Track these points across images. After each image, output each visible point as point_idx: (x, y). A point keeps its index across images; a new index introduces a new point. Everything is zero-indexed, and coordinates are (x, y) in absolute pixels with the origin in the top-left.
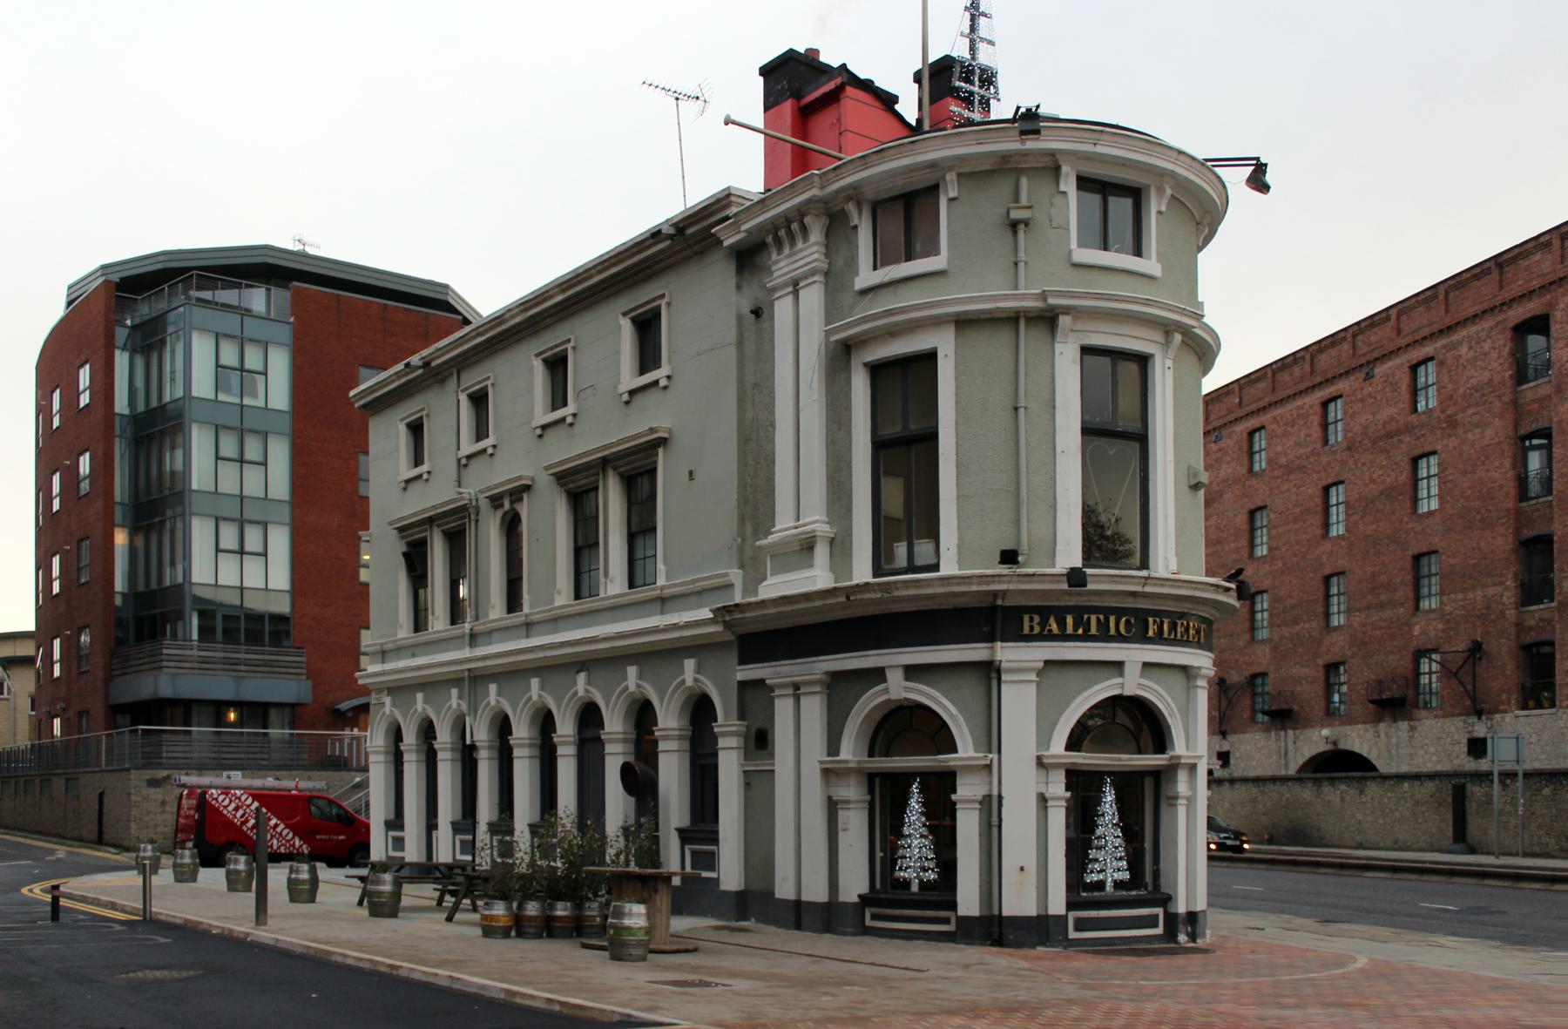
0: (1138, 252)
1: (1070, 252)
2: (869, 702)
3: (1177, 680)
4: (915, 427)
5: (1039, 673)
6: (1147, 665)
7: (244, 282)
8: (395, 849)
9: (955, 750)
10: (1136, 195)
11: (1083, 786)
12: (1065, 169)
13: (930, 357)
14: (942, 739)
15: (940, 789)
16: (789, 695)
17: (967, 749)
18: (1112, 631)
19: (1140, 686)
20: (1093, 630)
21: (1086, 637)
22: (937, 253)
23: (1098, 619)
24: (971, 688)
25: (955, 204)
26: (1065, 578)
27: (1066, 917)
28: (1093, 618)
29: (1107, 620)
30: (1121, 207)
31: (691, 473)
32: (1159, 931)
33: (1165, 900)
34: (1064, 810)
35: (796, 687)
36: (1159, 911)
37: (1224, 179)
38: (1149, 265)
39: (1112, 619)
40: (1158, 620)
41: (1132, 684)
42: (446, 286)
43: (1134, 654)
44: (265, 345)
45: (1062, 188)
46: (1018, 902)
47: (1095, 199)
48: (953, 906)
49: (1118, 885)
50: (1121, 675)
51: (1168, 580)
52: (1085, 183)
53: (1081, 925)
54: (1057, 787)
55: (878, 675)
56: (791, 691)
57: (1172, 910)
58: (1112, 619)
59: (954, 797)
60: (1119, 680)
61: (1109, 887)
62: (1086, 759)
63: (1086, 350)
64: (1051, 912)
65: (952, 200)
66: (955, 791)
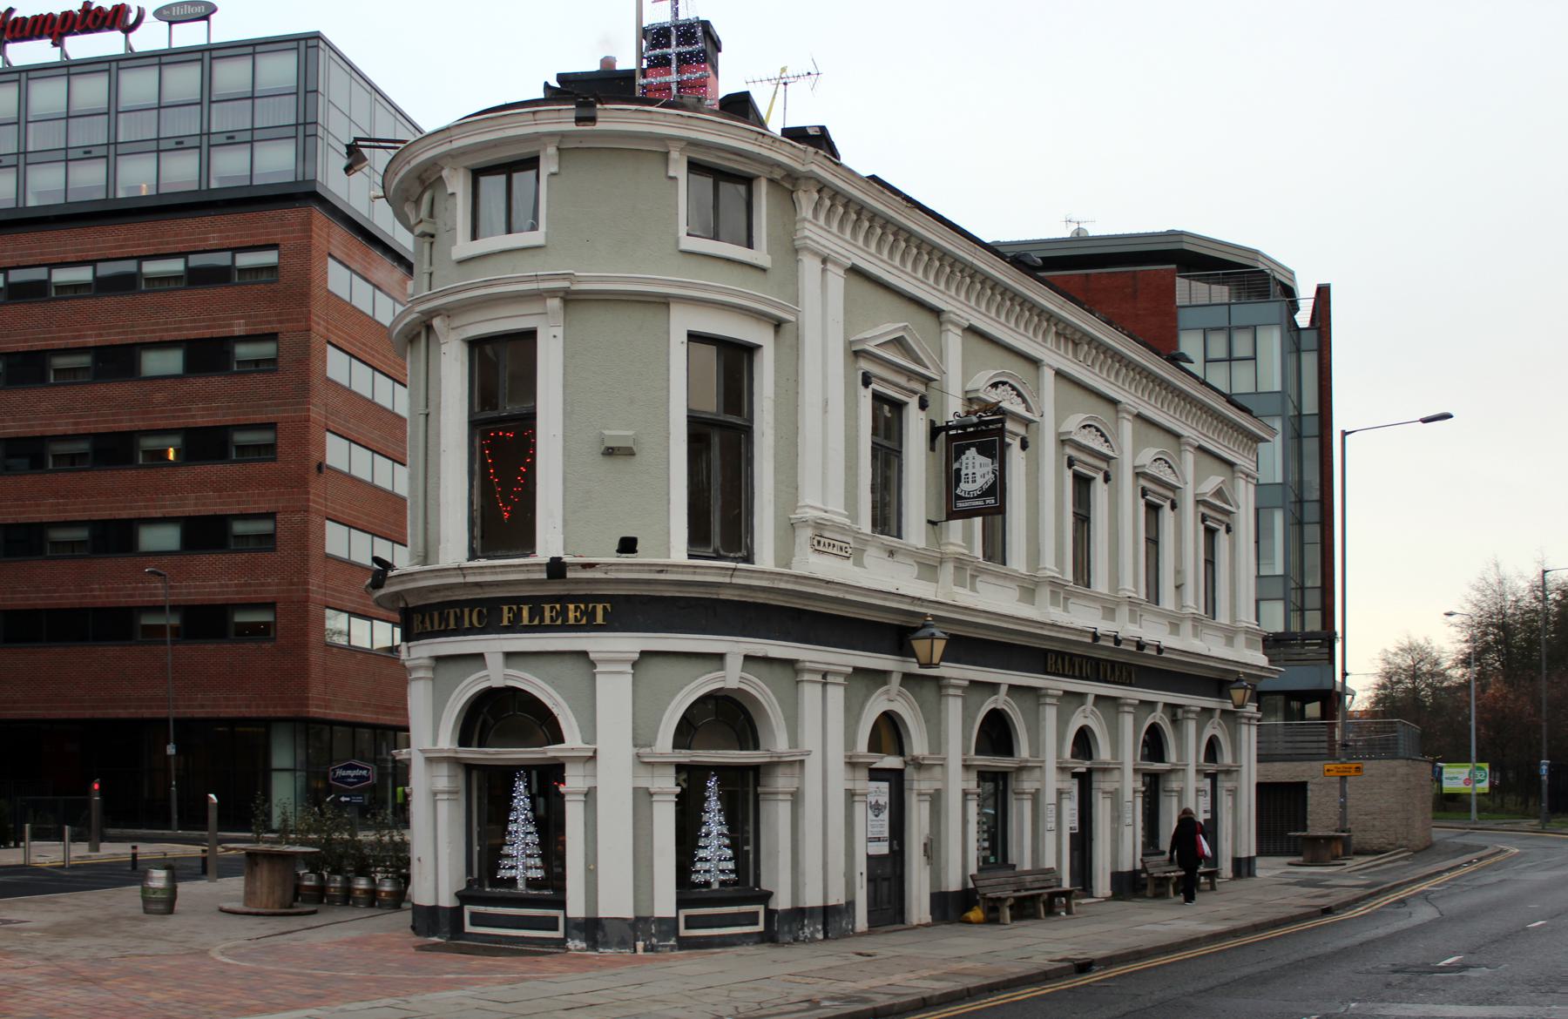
1: (677, 242)
3: (569, 670)
5: (635, 664)
6: (748, 658)
8: (738, 838)
9: (562, 741)
10: (748, 181)
11: (692, 779)
12: (674, 155)
13: (530, 335)
14: (546, 726)
15: (549, 778)
16: (818, 682)
18: (467, 625)
20: (600, 620)
21: (542, 628)
23: (605, 608)
25: (554, 179)
26: (545, 568)
27: (677, 918)
28: (600, 608)
29: (520, 610)
30: (732, 193)
31: (610, 452)
32: (760, 927)
33: (765, 897)
34: (673, 805)
35: (825, 675)
36: (761, 909)
37: (384, 166)
39: (466, 611)
40: (515, 607)
41: (497, 675)
42: (1256, 252)
43: (493, 645)
45: (671, 173)
46: (616, 903)
47: (708, 182)
48: (561, 904)
49: (531, 883)
50: (485, 667)
51: (772, 573)
52: (694, 167)
53: (691, 922)
54: (667, 784)
56: (819, 678)
57: (772, 906)
58: (466, 611)
59: (562, 789)
61: (521, 885)
62: (685, 756)
63: (475, 344)
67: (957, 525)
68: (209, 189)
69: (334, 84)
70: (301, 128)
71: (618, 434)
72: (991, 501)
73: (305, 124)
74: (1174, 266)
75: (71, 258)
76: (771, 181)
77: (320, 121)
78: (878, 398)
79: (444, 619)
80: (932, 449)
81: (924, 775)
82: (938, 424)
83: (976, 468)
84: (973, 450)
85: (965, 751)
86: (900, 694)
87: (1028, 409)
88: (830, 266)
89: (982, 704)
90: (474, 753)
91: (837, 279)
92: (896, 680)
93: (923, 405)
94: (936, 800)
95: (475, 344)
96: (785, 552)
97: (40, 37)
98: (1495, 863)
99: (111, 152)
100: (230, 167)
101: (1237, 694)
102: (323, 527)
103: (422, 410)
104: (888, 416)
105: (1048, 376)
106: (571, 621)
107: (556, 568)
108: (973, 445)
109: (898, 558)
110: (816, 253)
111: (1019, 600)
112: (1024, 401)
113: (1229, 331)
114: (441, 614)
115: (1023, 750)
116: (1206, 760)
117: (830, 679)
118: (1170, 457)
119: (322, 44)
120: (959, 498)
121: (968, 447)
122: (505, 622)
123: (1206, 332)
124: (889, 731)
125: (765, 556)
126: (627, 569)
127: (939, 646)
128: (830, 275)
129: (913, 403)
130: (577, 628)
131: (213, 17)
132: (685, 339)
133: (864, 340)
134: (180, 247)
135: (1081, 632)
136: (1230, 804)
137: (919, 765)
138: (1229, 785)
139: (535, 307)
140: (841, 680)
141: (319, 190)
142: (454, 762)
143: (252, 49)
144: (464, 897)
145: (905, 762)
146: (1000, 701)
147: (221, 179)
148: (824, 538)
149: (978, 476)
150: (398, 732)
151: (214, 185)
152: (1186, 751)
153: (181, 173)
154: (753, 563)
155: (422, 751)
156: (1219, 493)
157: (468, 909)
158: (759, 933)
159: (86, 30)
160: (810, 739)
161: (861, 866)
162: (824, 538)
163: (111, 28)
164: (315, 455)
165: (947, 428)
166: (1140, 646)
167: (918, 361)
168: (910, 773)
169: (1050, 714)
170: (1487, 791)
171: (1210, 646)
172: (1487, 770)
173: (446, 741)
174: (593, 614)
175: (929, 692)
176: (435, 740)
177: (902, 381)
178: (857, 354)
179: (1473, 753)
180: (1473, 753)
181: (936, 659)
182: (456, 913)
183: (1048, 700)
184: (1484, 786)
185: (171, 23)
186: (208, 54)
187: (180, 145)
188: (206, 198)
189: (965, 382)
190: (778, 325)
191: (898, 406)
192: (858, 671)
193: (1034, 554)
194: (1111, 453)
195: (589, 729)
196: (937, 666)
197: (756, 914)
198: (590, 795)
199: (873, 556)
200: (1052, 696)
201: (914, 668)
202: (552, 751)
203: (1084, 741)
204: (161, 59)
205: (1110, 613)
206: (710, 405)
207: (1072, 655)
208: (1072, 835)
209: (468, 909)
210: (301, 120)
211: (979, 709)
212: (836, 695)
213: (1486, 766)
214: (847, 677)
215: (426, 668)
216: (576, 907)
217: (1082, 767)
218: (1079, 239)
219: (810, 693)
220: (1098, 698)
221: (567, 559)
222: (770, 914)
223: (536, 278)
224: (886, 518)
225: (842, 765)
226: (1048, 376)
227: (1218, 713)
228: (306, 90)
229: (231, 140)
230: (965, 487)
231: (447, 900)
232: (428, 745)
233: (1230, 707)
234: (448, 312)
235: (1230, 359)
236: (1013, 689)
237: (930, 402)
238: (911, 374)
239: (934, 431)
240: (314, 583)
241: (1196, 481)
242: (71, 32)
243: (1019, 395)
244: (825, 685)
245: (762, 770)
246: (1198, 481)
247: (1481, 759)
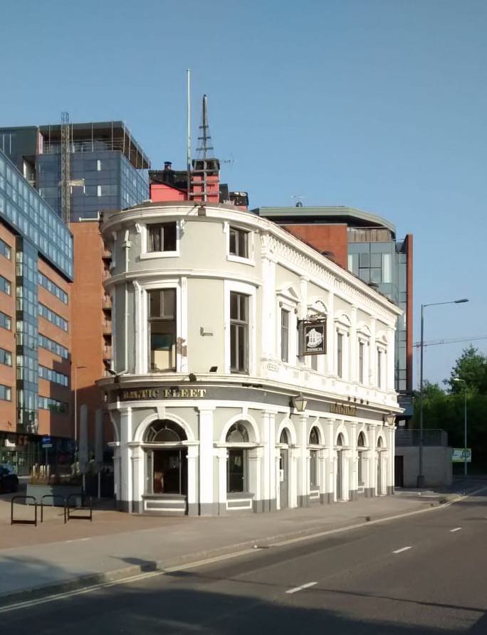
2: (152, 417)
5: (214, 411)
20: (202, 395)
35: (270, 414)
41: (163, 415)
43: (161, 404)
53: (230, 505)
59: (187, 457)
72: (320, 349)
74: (346, 224)
78: (283, 310)
83: (315, 337)
84: (314, 329)
91: (273, 266)
98: (214, 556)
106: (183, 396)
108: (313, 328)
110: (268, 259)
112: (325, 307)
120: (308, 347)
121: (312, 328)
126: (214, 377)
130: (194, 398)
137: (293, 447)
144: (145, 497)
146: (316, 423)
149: (316, 340)
158: (249, 510)
161: (278, 485)
173: (139, 438)
184: (469, 459)
193: (350, 375)
197: (249, 502)
199: (282, 369)
202: (184, 443)
208: (281, 482)
212: (273, 421)
213: (470, 450)
222: (255, 503)
223: (179, 270)
226: (331, 295)
230: (310, 344)
237: (299, 312)
241: (357, 323)
243: (324, 305)
246: (376, 331)
247: (468, 447)
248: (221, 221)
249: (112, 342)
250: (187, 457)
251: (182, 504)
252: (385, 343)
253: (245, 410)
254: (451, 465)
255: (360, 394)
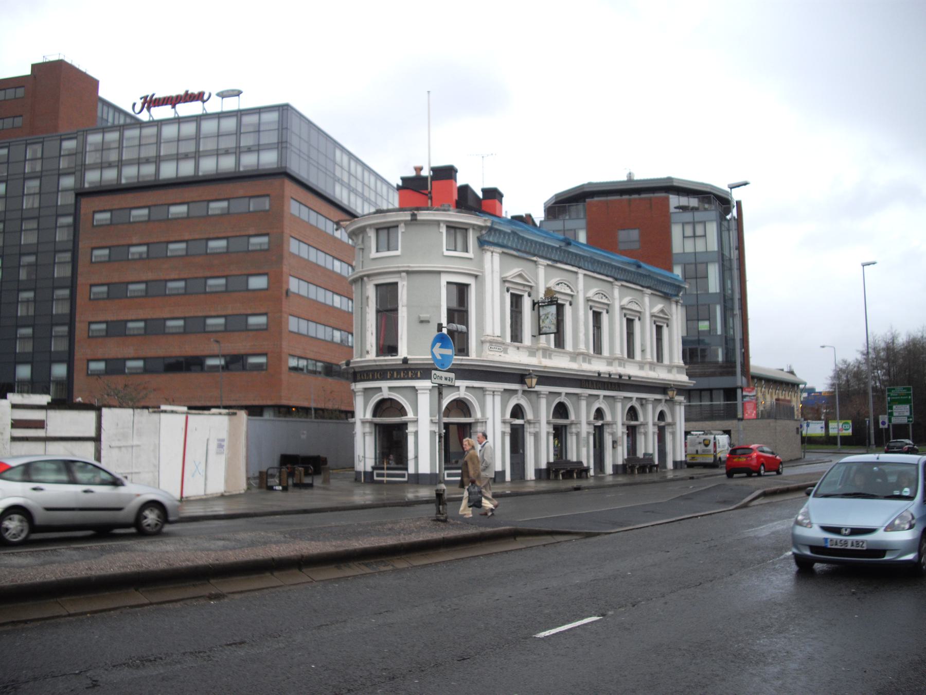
0: (467, 251)
1: (443, 253)
2: (377, 398)
4: (389, 307)
5: (430, 390)
7: (567, 204)
10: (466, 230)
14: (402, 411)
17: (410, 415)
19: (465, 394)
22: (397, 249)
24: (410, 393)
29: (393, 373)
31: (422, 322)
35: (494, 392)
38: (470, 255)
39: (376, 373)
41: (386, 394)
43: (385, 385)
44: (704, 223)
45: (441, 231)
48: (406, 469)
55: (379, 389)
56: (492, 393)
59: (407, 431)
60: (458, 393)
63: (377, 286)
64: (421, 471)
65: (402, 232)
66: (407, 429)
67: (543, 337)
68: (239, 171)
69: (295, 125)
70: (280, 144)
71: (424, 316)
73: (282, 142)
75: (178, 201)
76: (474, 229)
77: (288, 141)
79: (368, 375)
80: (534, 309)
81: (532, 426)
82: (536, 301)
85: (548, 416)
86: (522, 397)
87: (572, 291)
88: (494, 254)
89: (554, 400)
90: (378, 420)
92: (520, 393)
93: (529, 295)
94: (536, 436)
95: (377, 286)
96: (480, 351)
97: (166, 104)
99: (197, 156)
100: (249, 161)
101: (670, 393)
102: (288, 320)
103: (360, 306)
104: (516, 301)
105: (581, 277)
106: (410, 376)
107: (405, 361)
109: (521, 349)
111: (570, 361)
112: (570, 288)
113: (694, 224)
114: (367, 374)
115: (572, 417)
116: (659, 419)
117: (495, 393)
118: (606, 292)
119: (289, 108)
122: (389, 377)
123: (684, 224)
124: (518, 412)
125: (473, 354)
127: (534, 381)
128: (494, 257)
129: (526, 295)
131: (241, 95)
132: (446, 284)
133: (506, 277)
134: (226, 196)
135: (594, 372)
136: (671, 438)
137: (529, 422)
138: (670, 430)
139: (398, 275)
140: (500, 393)
141: (288, 171)
142: (371, 423)
143: (259, 111)
144: (374, 468)
145: (525, 422)
146: (562, 399)
147: (244, 166)
148: (495, 343)
150: (352, 414)
151: (241, 169)
152: (648, 417)
153: (227, 164)
154: (469, 356)
155: (360, 419)
156: (662, 311)
157: (375, 472)
159: (185, 101)
160: (489, 414)
162: (495, 343)
163: (197, 100)
164: (285, 287)
165: (538, 303)
166: (620, 376)
167: (529, 282)
168: (527, 426)
169: (583, 404)
170: (851, 434)
171: (661, 375)
172: (851, 424)
173: (369, 416)
174: (417, 374)
175: (534, 397)
176: (364, 416)
177: (521, 288)
178: (504, 281)
179: (838, 416)
180: (838, 416)
181: (533, 386)
182: (372, 473)
183: (583, 398)
185: (223, 98)
186: (239, 114)
187: (227, 152)
188: (237, 175)
189: (546, 284)
190: (476, 277)
191: (521, 296)
192: (505, 390)
194: (608, 302)
195: (416, 412)
196: (534, 387)
198: (416, 433)
200: (584, 396)
201: (526, 388)
202: (404, 419)
203: (599, 414)
204: (220, 116)
205: (610, 364)
206: (454, 305)
207: (592, 381)
209: (375, 472)
210: (280, 141)
211: (553, 402)
212: (498, 399)
214: (502, 392)
215: (362, 391)
216: (411, 470)
217: (599, 423)
218: (630, 180)
219: (489, 399)
220: (605, 397)
221: (409, 357)
223: (398, 267)
224: (516, 336)
225: (500, 423)
227: (663, 401)
228: (283, 127)
229: (249, 150)
231: (369, 469)
232: (362, 417)
233: (668, 398)
234: (368, 276)
235: (694, 236)
236: (567, 394)
237: (532, 294)
238: (524, 285)
239: (534, 304)
240: (285, 344)
242: (179, 102)
243: (568, 286)
244: (494, 395)
245: (472, 425)
248: (438, 223)
249: (51, 391)
250: (407, 431)
251: (459, 473)
252: (666, 317)
253: (462, 390)
254: (279, 456)
255: (632, 371)
